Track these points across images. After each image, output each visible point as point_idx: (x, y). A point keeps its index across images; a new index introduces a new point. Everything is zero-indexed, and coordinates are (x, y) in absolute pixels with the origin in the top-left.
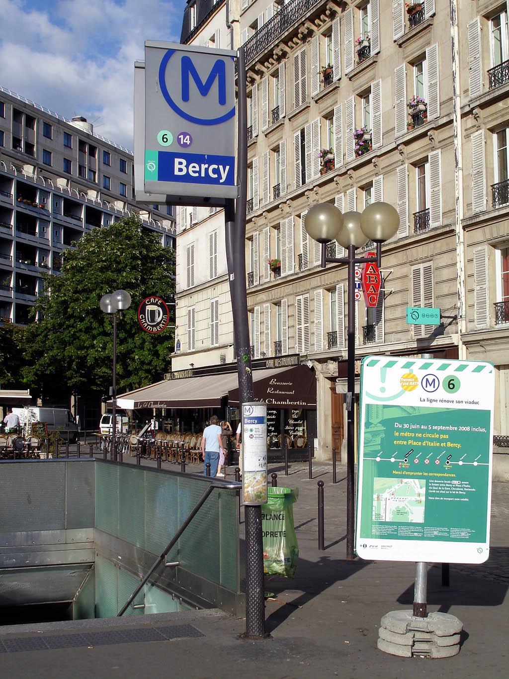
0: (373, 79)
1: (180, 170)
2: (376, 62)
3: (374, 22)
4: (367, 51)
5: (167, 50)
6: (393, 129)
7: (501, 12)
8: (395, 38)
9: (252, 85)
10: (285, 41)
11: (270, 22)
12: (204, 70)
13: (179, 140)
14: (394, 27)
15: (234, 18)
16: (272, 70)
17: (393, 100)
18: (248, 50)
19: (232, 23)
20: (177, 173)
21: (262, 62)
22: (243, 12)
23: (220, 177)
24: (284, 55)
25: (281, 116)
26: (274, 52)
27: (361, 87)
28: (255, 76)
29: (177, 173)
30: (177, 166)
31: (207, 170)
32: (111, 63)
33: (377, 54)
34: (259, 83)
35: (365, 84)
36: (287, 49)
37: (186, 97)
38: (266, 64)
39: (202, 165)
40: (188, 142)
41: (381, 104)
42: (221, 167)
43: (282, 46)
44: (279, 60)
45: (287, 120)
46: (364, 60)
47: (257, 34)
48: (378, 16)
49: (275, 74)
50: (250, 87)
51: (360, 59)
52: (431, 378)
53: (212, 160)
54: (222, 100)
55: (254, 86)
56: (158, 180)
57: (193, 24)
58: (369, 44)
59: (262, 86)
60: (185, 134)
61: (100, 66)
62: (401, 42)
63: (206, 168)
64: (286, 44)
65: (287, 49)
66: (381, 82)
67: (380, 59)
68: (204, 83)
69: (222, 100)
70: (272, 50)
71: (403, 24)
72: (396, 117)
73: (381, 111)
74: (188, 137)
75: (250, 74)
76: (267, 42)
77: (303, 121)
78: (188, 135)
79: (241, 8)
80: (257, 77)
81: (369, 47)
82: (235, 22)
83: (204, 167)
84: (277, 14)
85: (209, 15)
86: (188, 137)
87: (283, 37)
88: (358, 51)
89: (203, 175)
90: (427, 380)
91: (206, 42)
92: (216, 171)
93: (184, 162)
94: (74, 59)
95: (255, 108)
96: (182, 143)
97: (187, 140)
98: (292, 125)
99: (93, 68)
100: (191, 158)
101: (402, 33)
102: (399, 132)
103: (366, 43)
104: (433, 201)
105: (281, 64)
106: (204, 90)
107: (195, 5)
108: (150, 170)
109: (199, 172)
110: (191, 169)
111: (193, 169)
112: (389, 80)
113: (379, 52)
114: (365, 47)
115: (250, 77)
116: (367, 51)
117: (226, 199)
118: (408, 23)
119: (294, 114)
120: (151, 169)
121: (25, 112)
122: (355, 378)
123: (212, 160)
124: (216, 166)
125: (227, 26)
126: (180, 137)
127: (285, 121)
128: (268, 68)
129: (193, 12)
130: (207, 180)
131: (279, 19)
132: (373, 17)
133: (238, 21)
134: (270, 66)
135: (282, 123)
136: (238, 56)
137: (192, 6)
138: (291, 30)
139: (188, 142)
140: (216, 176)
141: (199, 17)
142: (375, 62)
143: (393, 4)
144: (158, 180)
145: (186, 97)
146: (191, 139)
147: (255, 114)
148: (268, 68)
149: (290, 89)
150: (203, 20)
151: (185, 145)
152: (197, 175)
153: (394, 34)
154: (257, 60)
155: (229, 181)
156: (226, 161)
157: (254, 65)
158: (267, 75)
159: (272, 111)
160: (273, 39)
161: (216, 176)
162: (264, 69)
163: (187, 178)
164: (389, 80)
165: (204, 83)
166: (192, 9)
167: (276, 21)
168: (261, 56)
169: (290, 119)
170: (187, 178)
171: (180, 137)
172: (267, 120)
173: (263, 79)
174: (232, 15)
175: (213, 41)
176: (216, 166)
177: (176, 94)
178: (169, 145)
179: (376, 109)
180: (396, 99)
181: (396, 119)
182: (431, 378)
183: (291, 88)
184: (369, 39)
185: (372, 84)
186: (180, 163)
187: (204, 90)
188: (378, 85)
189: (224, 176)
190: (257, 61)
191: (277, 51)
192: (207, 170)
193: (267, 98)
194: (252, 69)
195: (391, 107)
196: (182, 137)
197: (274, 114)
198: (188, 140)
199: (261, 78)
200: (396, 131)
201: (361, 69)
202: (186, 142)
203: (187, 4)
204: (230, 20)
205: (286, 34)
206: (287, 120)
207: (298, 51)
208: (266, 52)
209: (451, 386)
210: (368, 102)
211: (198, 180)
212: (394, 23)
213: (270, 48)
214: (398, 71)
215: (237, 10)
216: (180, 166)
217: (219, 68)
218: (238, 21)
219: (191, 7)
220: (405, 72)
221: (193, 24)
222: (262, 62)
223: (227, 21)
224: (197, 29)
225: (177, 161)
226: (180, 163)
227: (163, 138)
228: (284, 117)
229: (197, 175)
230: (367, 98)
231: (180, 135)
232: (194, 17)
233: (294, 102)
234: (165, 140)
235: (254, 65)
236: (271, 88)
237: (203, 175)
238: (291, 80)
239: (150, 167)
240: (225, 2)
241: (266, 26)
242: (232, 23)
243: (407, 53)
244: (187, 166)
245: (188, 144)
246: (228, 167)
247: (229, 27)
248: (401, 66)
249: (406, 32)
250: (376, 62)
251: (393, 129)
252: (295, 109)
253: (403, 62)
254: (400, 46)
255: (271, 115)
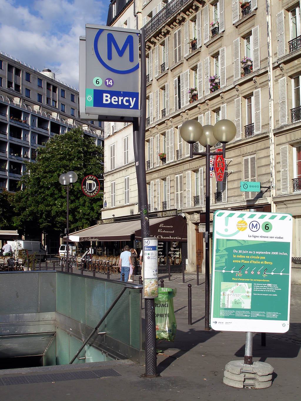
0: (221, 47)
1: (107, 100)
2: (223, 36)
3: (221, 13)
4: (217, 30)
5: (99, 30)
6: (233, 76)
7: (296, 7)
8: (234, 22)
9: (149, 50)
10: (169, 24)
11: (160, 13)
12: (121, 41)
13: (106, 83)
14: (233, 16)
15: (139, 10)
16: (161, 42)
17: (232, 59)
18: (147, 30)
19: (137, 13)
20: (104, 102)
21: (155, 36)
22: (144, 7)
23: (130, 105)
24: (168, 32)
25: (166, 69)
26: (162, 31)
27: (213, 51)
28: (151, 45)
29: (104, 102)
30: (105, 98)
31: (122, 100)
32: (66, 37)
33: (223, 32)
34: (153, 49)
35: (216, 50)
36: (170, 29)
37: (110, 57)
38: (157, 38)
39: (120, 98)
40: (111, 84)
41: (225, 61)
42: (131, 99)
43: (167, 27)
44: (165, 35)
45: (169, 71)
46: (215, 36)
47: (152, 20)
48: (224, 10)
49: (163, 44)
50: (148, 51)
51: (213, 35)
52: (255, 224)
53: (125, 94)
54: (132, 59)
55: (150, 51)
56: (94, 106)
57: (114, 14)
58: (219, 26)
59: (155, 51)
60: (109, 79)
61: (59, 39)
62: (237, 25)
63: (122, 99)
64: (169, 26)
65: (170, 29)
66: (225, 49)
67: (225, 35)
68: (121, 49)
69: (132, 59)
70: (161, 29)
71: (238, 14)
72: (234, 69)
73: (225, 65)
74: (111, 81)
75: (148, 44)
76: (158, 25)
77: (179, 71)
78: (111, 79)
79: (142, 5)
80: (152, 46)
81: (218, 28)
82: (139, 13)
83: (120, 98)
84: (164, 8)
85: (124, 9)
86: (111, 81)
87: (167, 22)
88: (212, 30)
89: (120, 103)
90: (253, 224)
91: (122, 25)
92: (127, 101)
93: (109, 96)
94: (44, 35)
95: (151, 64)
96: (108, 84)
97: (110, 83)
98: (173, 74)
99: (55, 40)
100: (113, 94)
101: (238, 20)
102: (236, 78)
103: (216, 26)
104: (256, 119)
105: (166, 38)
106: (121, 53)
107: (115, 3)
108: (89, 100)
109: (118, 102)
110: (113, 100)
111: (114, 100)
112: (230, 47)
113: (224, 31)
114: (216, 28)
115: (148, 46)
116: (217, 30)
117: (133, 117)
118: (241, 14)
119: (174, 67)
120: (89, 100)
121: (15, 66)
122: (210, 223)
123: (125, 94)
124: (127, 98)
125: (134, 16)
126: (106, 81)
127: (169, 72)
128: (159, 40)
129: (114, 7)
130: (122, 106)
131: (165, 11)
132: (221, 10)
133: (141, 12)
134: (160, 39)
135: (167, 72)
136: (141, 33)
137: (114, 4)
138: (172, 18)
139: (111, 84)
140: (128, 104)
141: (117, 10)
142: (222, 37)
143: (233, 2)
144: (94, 106)
145: (110, 57)
146: (113, 82)
147: (151, 67)
148: (159, 40)
149: (171, 52)
150: (120, 12)
151: (109, 86)
152: (116, 103)
153: (233, 20)
154: (152, 35)
155: (136, 107)
156: (134, 95)
157: (150, 39)
158: (158, 44)
159: (161, 66)
160: (162, 23)
161: (128, 104)
162: (156, 41)
163: (111, 105)
164: (230, 47)
165: (121, 49)
166: (114, 5)
167: (163, 12)
168: (154, 33)
169: (171, 70)
170: (111, 105)
171: (106, 81)
172: (158, 71)
173: (156, 47)
174: (137, 9)
175: (126, 24)
176: (127, 98)
177: (104, 55)
178: (100, 86)
179: (223, 64)
180: (234, 59)
181: (234, 71)
182: (255, 224)
183: (172, 52)
184: (218, 23)
185: (220, 50)
186: (107, 96)
187: (121, 53)
188: (223, 50)
189: (132, 104)
190: (152, 36)
191: (164, 30)
192: (122, 100)
193: (158, 58)
194: (149, 41)
195: (231, 63)
196: (107, 81)
197: (162, 67)
198: (111, 82)
199: (154, 46)
200: (234, 77)
201: (213, 41)
202: (110, 84)
203: (111, 2)
204: (136, 12)
205: (169, 20)
206: (169, 71)
207: (176, 30)
208: (157, 30)
209: (267, 228)
210: (217, 60)
211: (117, 106)
212: (233, 14)
213: (159, 29)
214: (235, 42)
215: (140, 6)
216: (106, 98)
217: (130, 40)
218: (141, 12)
219: (113, 4)
220: (239, 42)
221: (114, 14)
222: (155, 36)
223: (134, 12)
224: (117, 17)
225: (105, 95)
226: (107, 96)
227: (96, 82)
228: (168, 69)
229: (116, 103)
230: (217, 58)
231: (107, 80)
232: (115, 10)
233: (174, 60)
234: (98, 83)
235: (150, 39)
236: (160, 52)
237: (120, 103)
238: (172, 47)
239: (89, 99)
240: (133, 1)
241: (157, 15)
242: (137, 13)
243: (240, 32)
244: (111, 98)
245: (111, 85)
246: (135, 99)
247: (135, 16)
248: (237, 39)
249: (240, 19)
250: (223, 36)
251: (233, 76)
252: (174, 64)
253: (238, 37)
254: (237, 27)
255: (160, 68)
